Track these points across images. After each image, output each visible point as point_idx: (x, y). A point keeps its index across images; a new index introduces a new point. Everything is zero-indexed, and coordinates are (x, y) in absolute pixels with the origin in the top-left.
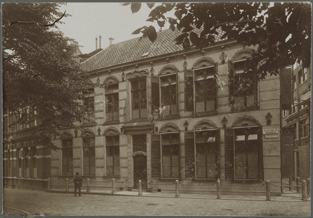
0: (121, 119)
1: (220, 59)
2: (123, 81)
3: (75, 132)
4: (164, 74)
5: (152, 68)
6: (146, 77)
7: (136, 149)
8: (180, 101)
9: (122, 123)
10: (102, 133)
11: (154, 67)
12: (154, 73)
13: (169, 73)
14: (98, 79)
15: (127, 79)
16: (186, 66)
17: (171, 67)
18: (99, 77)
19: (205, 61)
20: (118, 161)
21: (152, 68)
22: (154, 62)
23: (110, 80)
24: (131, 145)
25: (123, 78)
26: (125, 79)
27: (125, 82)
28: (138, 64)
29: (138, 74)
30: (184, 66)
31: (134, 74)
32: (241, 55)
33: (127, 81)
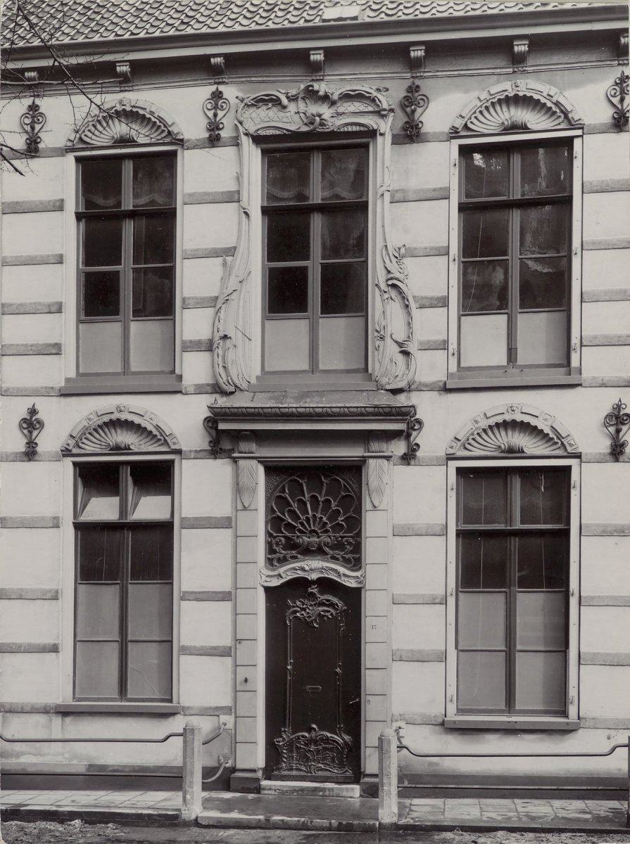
0: (195, 368)
1: (202, 114)
2: (214, 140)
3: (118, 419)
4: (486, 132)
5: (413, 89)
6: (372, 133)
7: (291, 545)
8: (184, 300)
9: (200, 390)
10: (49, 441)
11: (427, 86)
12: (40, 135)
13: (524, 128)
14: (34, 108)
15: (246, 134)
16: (37, 127)
17: (536, 97)
18: (38, 101)
19: (132, 115)
20: (167, 616)
21: (413, 89)
22: (437, 51)
23: (120, 128)
24: (257, 522)
25: (214, 127)
26: (225, 134)
27: (228, 152)
28: (226, 56)
29: (326, 111)
30: (616, 100)
31: (292, 107)
32: (110, 121)
33: (246, 142)
